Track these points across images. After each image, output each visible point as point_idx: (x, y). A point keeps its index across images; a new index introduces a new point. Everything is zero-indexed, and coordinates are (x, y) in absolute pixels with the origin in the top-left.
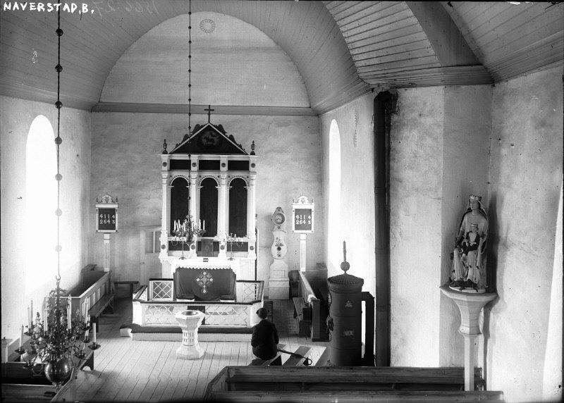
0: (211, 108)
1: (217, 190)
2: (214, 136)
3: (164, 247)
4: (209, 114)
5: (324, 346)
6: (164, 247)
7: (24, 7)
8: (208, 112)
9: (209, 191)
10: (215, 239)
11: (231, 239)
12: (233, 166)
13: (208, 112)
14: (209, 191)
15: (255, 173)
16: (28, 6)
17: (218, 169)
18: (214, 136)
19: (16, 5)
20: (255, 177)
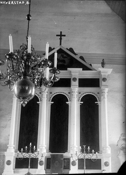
0: (63, 34)
1: (67, 106)
2: (65, 57)
3: (9, 163)
4: (61, 39)
5: (102, 82)
6: (9, 163)
7: (7, 3)
8: (59, 37)
9: (60, 107)
10: (66, 155)
11: (82, 156)
12: (84, 83)
13: (59, 37)
14: (60, 107)
15: (106, 86)
16: (8, 3)
17: (81, 161)
18: (65, 57)
19: (12, 3)
20: (106, 90)
